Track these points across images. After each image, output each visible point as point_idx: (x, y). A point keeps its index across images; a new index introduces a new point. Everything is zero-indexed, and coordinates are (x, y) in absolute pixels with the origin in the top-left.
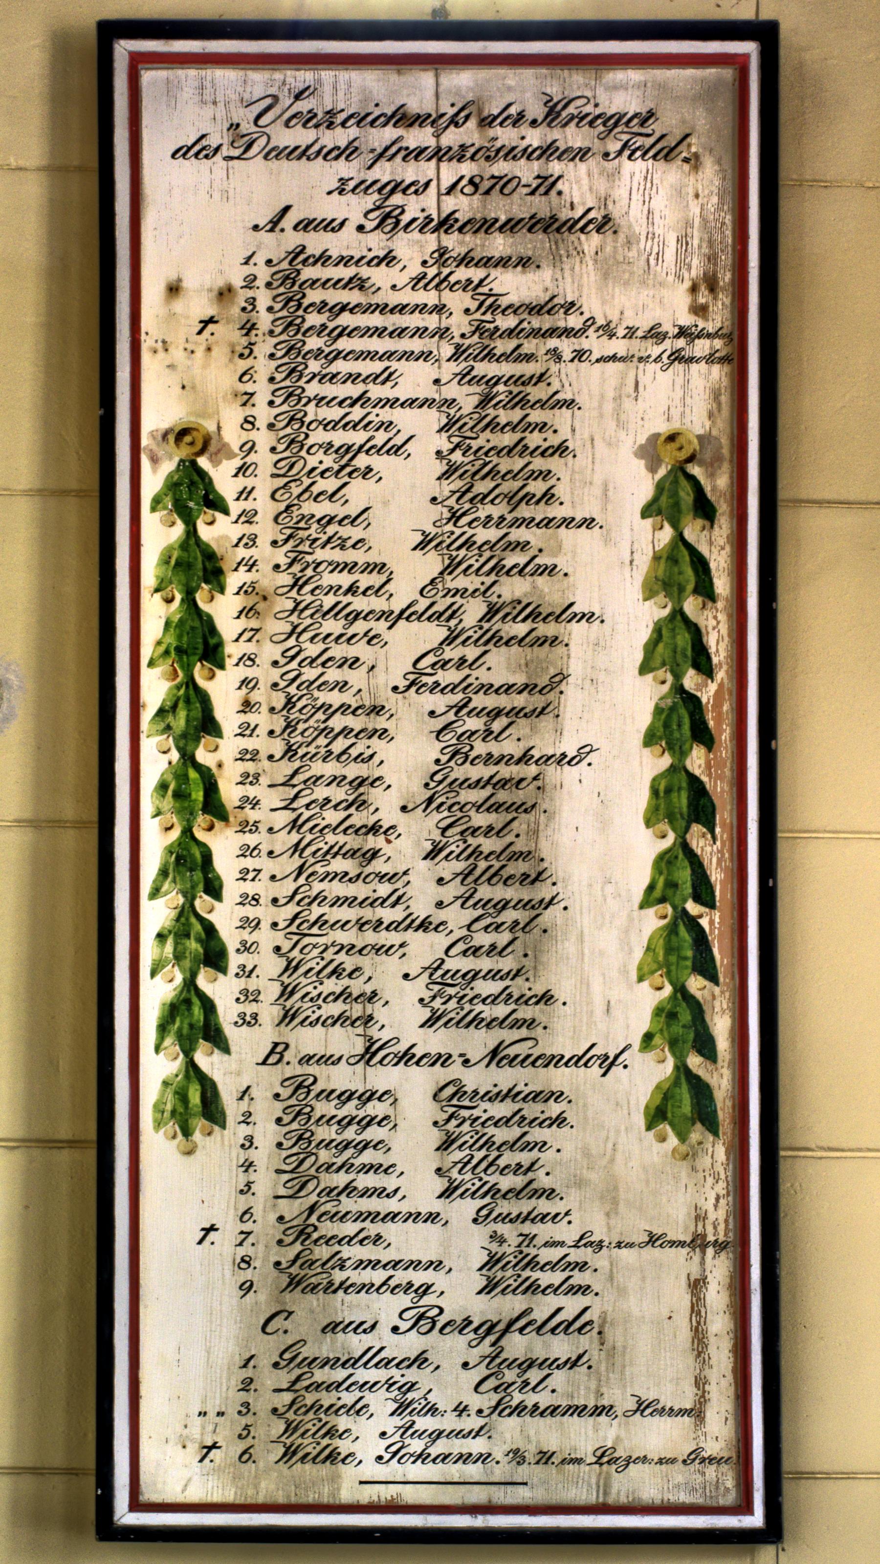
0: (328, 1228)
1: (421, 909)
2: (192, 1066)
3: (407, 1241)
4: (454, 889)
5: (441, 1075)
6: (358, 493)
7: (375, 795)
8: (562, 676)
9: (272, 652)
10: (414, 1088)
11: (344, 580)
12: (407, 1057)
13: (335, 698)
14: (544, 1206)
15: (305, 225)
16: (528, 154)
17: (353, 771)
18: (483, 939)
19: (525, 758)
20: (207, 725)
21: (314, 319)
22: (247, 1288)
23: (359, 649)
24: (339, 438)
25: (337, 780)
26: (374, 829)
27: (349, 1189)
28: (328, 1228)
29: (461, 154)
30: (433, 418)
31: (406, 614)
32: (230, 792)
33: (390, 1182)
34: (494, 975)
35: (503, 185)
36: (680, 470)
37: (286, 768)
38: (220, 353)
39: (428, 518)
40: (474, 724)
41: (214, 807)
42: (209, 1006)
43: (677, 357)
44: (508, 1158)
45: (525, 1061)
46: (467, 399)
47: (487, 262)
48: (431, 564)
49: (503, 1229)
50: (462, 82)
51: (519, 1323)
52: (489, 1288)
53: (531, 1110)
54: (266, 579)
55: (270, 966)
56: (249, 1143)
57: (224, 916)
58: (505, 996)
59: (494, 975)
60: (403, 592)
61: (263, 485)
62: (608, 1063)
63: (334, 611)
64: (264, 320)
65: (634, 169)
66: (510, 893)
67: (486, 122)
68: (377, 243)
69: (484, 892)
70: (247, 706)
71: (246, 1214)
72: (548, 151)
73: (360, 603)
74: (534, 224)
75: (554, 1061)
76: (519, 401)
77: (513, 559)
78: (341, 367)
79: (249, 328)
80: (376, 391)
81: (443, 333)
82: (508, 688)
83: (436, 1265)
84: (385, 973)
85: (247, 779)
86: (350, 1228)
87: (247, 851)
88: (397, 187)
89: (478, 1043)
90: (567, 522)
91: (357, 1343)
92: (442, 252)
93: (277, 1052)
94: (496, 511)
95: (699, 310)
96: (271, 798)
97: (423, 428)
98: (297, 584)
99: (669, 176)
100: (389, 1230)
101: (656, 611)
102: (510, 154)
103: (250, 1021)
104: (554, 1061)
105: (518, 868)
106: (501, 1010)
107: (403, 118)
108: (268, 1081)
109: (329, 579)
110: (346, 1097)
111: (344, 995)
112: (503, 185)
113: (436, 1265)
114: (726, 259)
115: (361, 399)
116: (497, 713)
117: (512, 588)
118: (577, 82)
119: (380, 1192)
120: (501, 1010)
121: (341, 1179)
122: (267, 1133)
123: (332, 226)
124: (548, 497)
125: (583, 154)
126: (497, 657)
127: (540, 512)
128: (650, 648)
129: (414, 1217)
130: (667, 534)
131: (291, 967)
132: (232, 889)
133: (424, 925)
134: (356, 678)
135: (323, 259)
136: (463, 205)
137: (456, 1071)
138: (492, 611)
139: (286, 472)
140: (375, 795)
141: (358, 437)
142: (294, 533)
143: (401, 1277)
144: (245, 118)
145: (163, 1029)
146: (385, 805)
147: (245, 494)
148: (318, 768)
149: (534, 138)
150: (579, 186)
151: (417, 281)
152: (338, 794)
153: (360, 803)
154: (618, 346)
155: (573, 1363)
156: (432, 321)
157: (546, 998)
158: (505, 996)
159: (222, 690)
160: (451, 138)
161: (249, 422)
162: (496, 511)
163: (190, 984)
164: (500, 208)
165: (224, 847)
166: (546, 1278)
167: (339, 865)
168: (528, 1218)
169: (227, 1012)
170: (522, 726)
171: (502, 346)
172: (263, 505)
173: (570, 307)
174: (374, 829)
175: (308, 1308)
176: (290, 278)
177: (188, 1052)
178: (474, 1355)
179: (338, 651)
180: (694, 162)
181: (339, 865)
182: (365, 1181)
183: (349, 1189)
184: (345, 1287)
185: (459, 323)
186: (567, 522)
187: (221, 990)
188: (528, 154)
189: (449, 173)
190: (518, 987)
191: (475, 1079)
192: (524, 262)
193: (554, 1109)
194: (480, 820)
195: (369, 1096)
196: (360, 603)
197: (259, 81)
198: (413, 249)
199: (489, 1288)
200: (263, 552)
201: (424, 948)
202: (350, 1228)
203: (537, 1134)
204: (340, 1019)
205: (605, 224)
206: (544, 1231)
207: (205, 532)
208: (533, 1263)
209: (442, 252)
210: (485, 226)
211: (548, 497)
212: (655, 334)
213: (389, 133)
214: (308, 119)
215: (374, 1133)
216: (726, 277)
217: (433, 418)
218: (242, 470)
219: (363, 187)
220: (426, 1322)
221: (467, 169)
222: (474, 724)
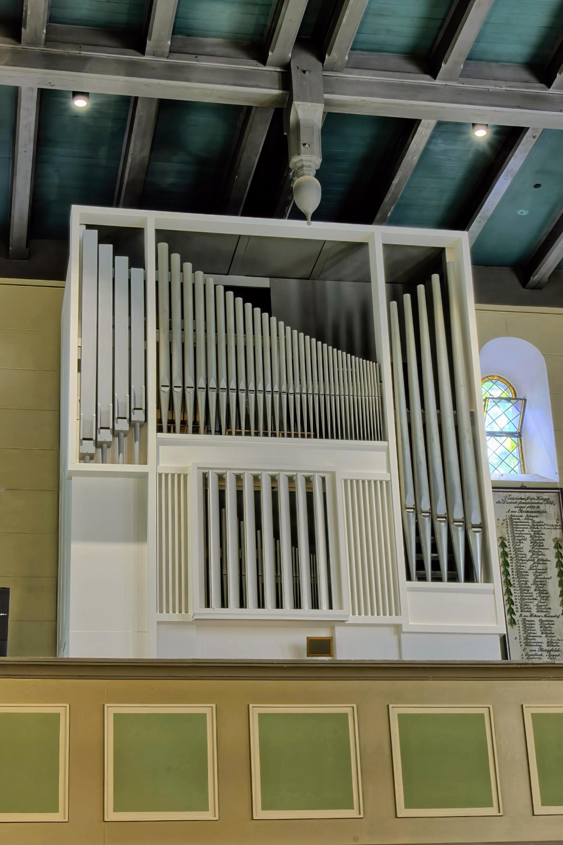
0: (529, 638)
1: (535, 597)
2: (511, 617)
3: (538, 640)
4: (538, 595)
5: (539, 618)
6: (522, 545)
7: (528, 583)
8: (547, 568)
9: (514, 568)
10: (537, 620)
11: (521, 556)
12: (535, 616)
13: (522, 571)
14: (553, 635)
15: (512, 512)
16: (536, 503)
17: (525, 580)
18: (542, 601)
19: (544, 578)
20: (509, 574)
21: (514, 523)
22: (521, 645)
23: (524, 564)
24: (519, 538)
25: (523, 581)
26: (528, 587)
27: (531, 633)
28: (529, 638)
29: (528, 503)
30: (529, 536)
31: (529, 560)
32: (512, 583)
33: (535, 632)
34: (544, 606)
35: (533, 507)
36: (557, 542)
37: (518, 579)
38: (504, 528)
39: (530, 548)
40: (538, 574)
41: (511, 585)
42: (513, 609)
43: (555, 528)
44: (548, 629)
45: (549, 617)
46: (532, 533)
47: (532, 516)
48: (531, 554)
49: (549, 638)
50: (527, 495)
51: (552, 650)
52: (548, 646)
53: (550, 623)
54: (513, 556)
55: (519, 604)
56: (519, 627)
57: (513, 598)
58: (545, 608)
59: (544, 606)
60: (528, 558)
61: (511, 544)
62: (558, 617)
63: (521, 560)
64: (509, 524)
65: (548, 505)
66: (545, 595)
67: (531, 499)
68: (520, 514)
69: (542, 595)
70: (513, 572)
71: (520, 636)
72: (538, 503)
73: (524, 559)
74: (539, 512)
75: (552, 617)
76: (538, 534)
77: (540, 553)
78: (518, 529)
79: (507, 525)
80: (522, 532)
81: (529, 525)
82: (541, 570)
83: (542, 643)
84: (531, 605)
85: (514, 581)
86: (531, 638)
87: (515, 590)
88: (522, 507)
89: (543, 614)
90: (545, 549)
91: (534, 653)
92: (527, 515)
93: (521, 615)
94: (538, 547)
95: (557, 523)
96: (517, 583)
97: (528, 537)
98: (516, 556)
99: (552, 506)
100: (536, 638)
101: (556, 560)
102: (534, 503)
103: (517, 611)
104: (552, 617)
105: (545, 592)
106: (545, 610)
107: (521, 499)
108: (520, 619)
109: (520, 556)
110: (529, 621)
111: (527, 608)
112: (533, 507)
113: (542, 643)
114: (560, 516)
115: (521, 533)
116: (540, 573)
117: (540, 557)
118: (540, 495)
119: (534, 633)
120: (545, 610)
121: (530, 632)
122: (521, 626)
123: (515, 512)
124: (543, 546)
125: (542, 503)
126: (539, 565)
127: (542, 547)
128: (557, 564)
129: (538, 636)
130: (557, 551)
131: (521, 604)
132: (514, 595)
133: (535, 599)
134: (524, 568)
135: (514, 516)
136: (529, 510)
137: (541, 618)
138: (538, 560)
139: (513, 542)
140: (528, 583)
141: (521, 538)
142: (516, 550)
143: (538, 644)
144: (504, 499)
145: (508, 612)
146: (529, 584)
147: (509, 545)
148: (521, 579)
149: (536, 501)
150: (542, 507)
151: (525, 519)
152: (524, 583)
153: (526, 584)
154: (549, 527)
155: (559, 655)
156: (527, 524)
157: (550, 609)
158: (545, 608)
159: (509, 569)
160: (527, 501)
161: (509, 536)
162: (538, 547)
163: (510, 606)
164: (533, 510)
165: (512, 589)
166: (554, 644)
167: (525, 592)
168: (551, 637)
169: (515, 610)
170: (543, 574)
171: (536, 527)
172: (512, 547)
173: (543, 522)
174: (528, 587)
175: (529, 648)
176: (511, 518)
177: (511, 615)
178: (547, 654)
179: (522, 565)
180: (554, 504)
181: (525, 592)
182: (533, 632)
183: (531, 633)
184: (532, 645)
185: (531, 524)
186: (545, 549)
187: (514, 607)
188: (536, 503)
189: (527, 505)
190: (547, 607)
191: (544, 619)
192: (537, 517)
193: (552, 623)
194: (540, 586)
195: (532, 621)
196: (524, 559)
197: (505, 494)
198: (524, 515)
199: (548, 646)
200: (512, 552)
201: (536, 602)
202: (531, 638)
203: (551, 626)
204: (527, 611)
205: (545, 512)
206: (553, 638)
207: (505, 550)
208: (552, 642)
209: (527, 515)
210: (532, 512)
211: (543, 546)
212: (553, 526)
213: (520, 501)
214: (511, 499)
215: (533, 626)
216: (560, 518)
217: (529, 536)
218: (508, 542)
219: (518, 507)
220: (541, 650)
221: (529, 505)
222: (538, 574)
